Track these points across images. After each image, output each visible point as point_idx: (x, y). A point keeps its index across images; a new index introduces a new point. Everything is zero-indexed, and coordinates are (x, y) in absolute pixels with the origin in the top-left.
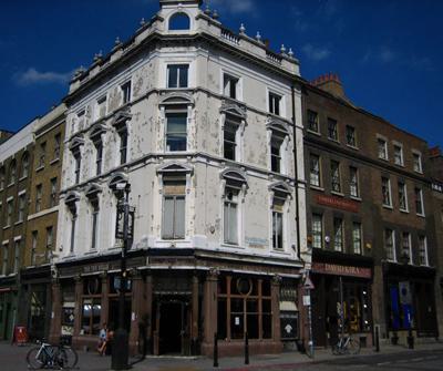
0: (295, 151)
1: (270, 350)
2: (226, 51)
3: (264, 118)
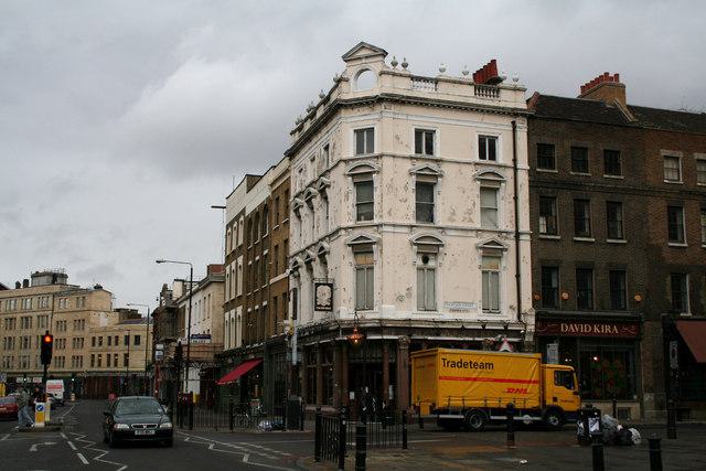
0: (516, 198)
2: (416, 103)
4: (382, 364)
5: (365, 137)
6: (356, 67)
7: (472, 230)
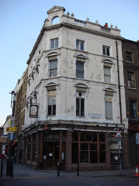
0: (118, 71)
1: (105, 169)
3: (100, 57)
4: (59, 142)
5: (54, 41)
6: (53, 15)
7: (101, 83)
